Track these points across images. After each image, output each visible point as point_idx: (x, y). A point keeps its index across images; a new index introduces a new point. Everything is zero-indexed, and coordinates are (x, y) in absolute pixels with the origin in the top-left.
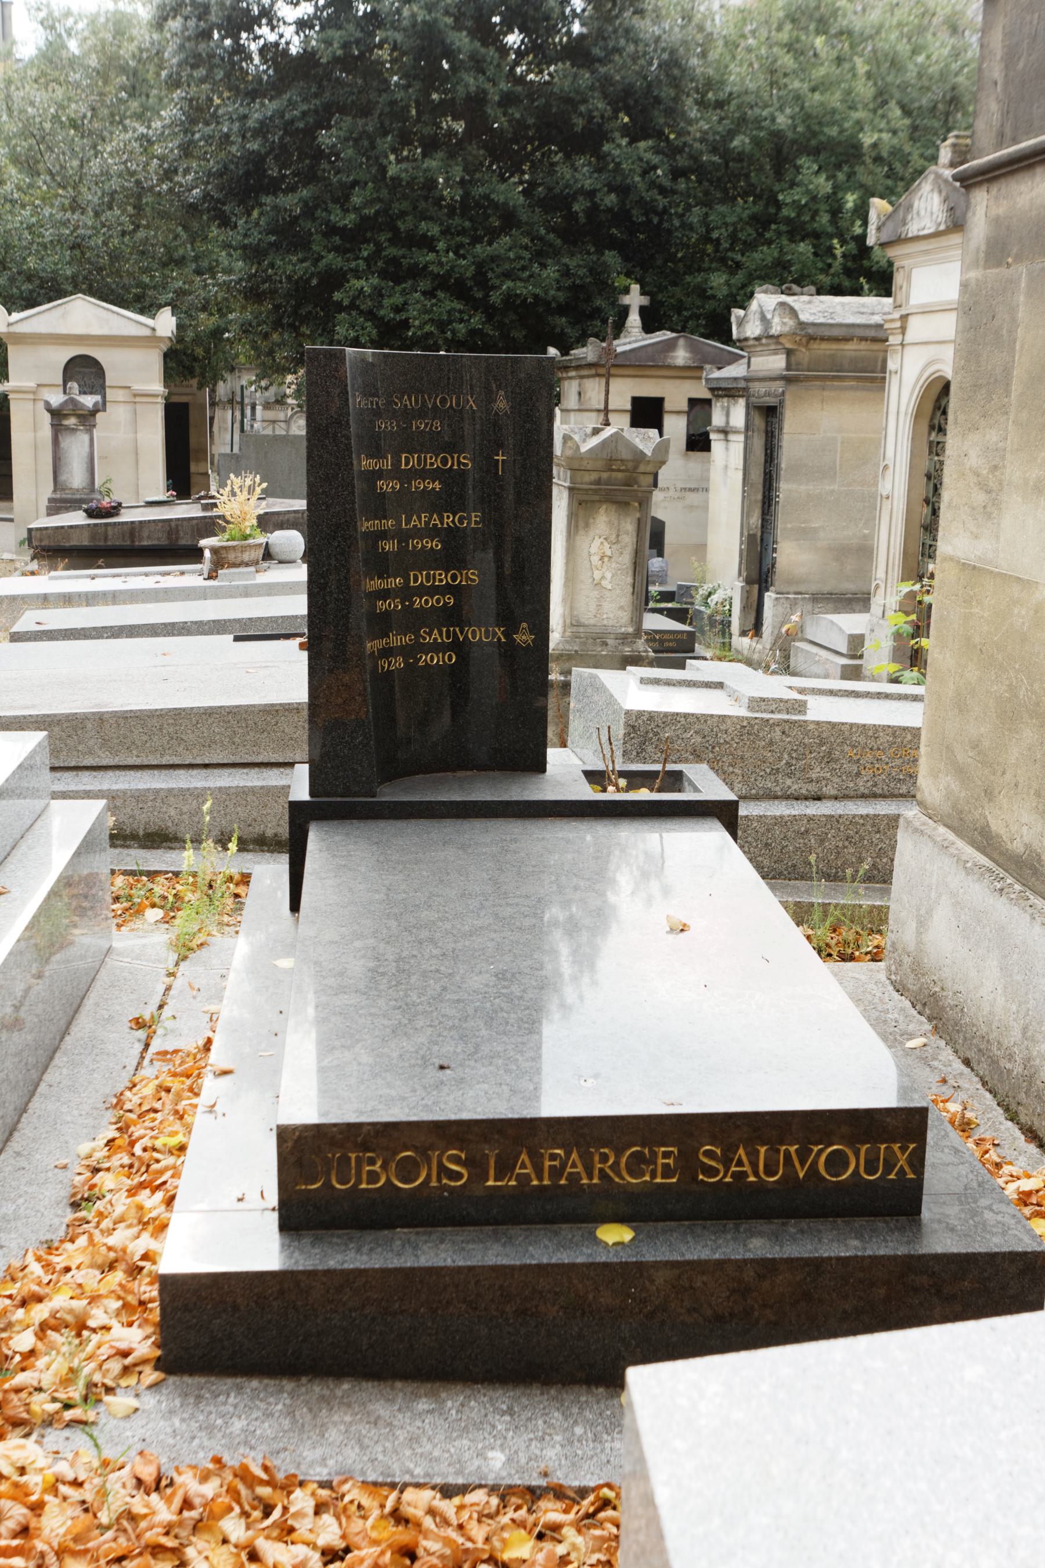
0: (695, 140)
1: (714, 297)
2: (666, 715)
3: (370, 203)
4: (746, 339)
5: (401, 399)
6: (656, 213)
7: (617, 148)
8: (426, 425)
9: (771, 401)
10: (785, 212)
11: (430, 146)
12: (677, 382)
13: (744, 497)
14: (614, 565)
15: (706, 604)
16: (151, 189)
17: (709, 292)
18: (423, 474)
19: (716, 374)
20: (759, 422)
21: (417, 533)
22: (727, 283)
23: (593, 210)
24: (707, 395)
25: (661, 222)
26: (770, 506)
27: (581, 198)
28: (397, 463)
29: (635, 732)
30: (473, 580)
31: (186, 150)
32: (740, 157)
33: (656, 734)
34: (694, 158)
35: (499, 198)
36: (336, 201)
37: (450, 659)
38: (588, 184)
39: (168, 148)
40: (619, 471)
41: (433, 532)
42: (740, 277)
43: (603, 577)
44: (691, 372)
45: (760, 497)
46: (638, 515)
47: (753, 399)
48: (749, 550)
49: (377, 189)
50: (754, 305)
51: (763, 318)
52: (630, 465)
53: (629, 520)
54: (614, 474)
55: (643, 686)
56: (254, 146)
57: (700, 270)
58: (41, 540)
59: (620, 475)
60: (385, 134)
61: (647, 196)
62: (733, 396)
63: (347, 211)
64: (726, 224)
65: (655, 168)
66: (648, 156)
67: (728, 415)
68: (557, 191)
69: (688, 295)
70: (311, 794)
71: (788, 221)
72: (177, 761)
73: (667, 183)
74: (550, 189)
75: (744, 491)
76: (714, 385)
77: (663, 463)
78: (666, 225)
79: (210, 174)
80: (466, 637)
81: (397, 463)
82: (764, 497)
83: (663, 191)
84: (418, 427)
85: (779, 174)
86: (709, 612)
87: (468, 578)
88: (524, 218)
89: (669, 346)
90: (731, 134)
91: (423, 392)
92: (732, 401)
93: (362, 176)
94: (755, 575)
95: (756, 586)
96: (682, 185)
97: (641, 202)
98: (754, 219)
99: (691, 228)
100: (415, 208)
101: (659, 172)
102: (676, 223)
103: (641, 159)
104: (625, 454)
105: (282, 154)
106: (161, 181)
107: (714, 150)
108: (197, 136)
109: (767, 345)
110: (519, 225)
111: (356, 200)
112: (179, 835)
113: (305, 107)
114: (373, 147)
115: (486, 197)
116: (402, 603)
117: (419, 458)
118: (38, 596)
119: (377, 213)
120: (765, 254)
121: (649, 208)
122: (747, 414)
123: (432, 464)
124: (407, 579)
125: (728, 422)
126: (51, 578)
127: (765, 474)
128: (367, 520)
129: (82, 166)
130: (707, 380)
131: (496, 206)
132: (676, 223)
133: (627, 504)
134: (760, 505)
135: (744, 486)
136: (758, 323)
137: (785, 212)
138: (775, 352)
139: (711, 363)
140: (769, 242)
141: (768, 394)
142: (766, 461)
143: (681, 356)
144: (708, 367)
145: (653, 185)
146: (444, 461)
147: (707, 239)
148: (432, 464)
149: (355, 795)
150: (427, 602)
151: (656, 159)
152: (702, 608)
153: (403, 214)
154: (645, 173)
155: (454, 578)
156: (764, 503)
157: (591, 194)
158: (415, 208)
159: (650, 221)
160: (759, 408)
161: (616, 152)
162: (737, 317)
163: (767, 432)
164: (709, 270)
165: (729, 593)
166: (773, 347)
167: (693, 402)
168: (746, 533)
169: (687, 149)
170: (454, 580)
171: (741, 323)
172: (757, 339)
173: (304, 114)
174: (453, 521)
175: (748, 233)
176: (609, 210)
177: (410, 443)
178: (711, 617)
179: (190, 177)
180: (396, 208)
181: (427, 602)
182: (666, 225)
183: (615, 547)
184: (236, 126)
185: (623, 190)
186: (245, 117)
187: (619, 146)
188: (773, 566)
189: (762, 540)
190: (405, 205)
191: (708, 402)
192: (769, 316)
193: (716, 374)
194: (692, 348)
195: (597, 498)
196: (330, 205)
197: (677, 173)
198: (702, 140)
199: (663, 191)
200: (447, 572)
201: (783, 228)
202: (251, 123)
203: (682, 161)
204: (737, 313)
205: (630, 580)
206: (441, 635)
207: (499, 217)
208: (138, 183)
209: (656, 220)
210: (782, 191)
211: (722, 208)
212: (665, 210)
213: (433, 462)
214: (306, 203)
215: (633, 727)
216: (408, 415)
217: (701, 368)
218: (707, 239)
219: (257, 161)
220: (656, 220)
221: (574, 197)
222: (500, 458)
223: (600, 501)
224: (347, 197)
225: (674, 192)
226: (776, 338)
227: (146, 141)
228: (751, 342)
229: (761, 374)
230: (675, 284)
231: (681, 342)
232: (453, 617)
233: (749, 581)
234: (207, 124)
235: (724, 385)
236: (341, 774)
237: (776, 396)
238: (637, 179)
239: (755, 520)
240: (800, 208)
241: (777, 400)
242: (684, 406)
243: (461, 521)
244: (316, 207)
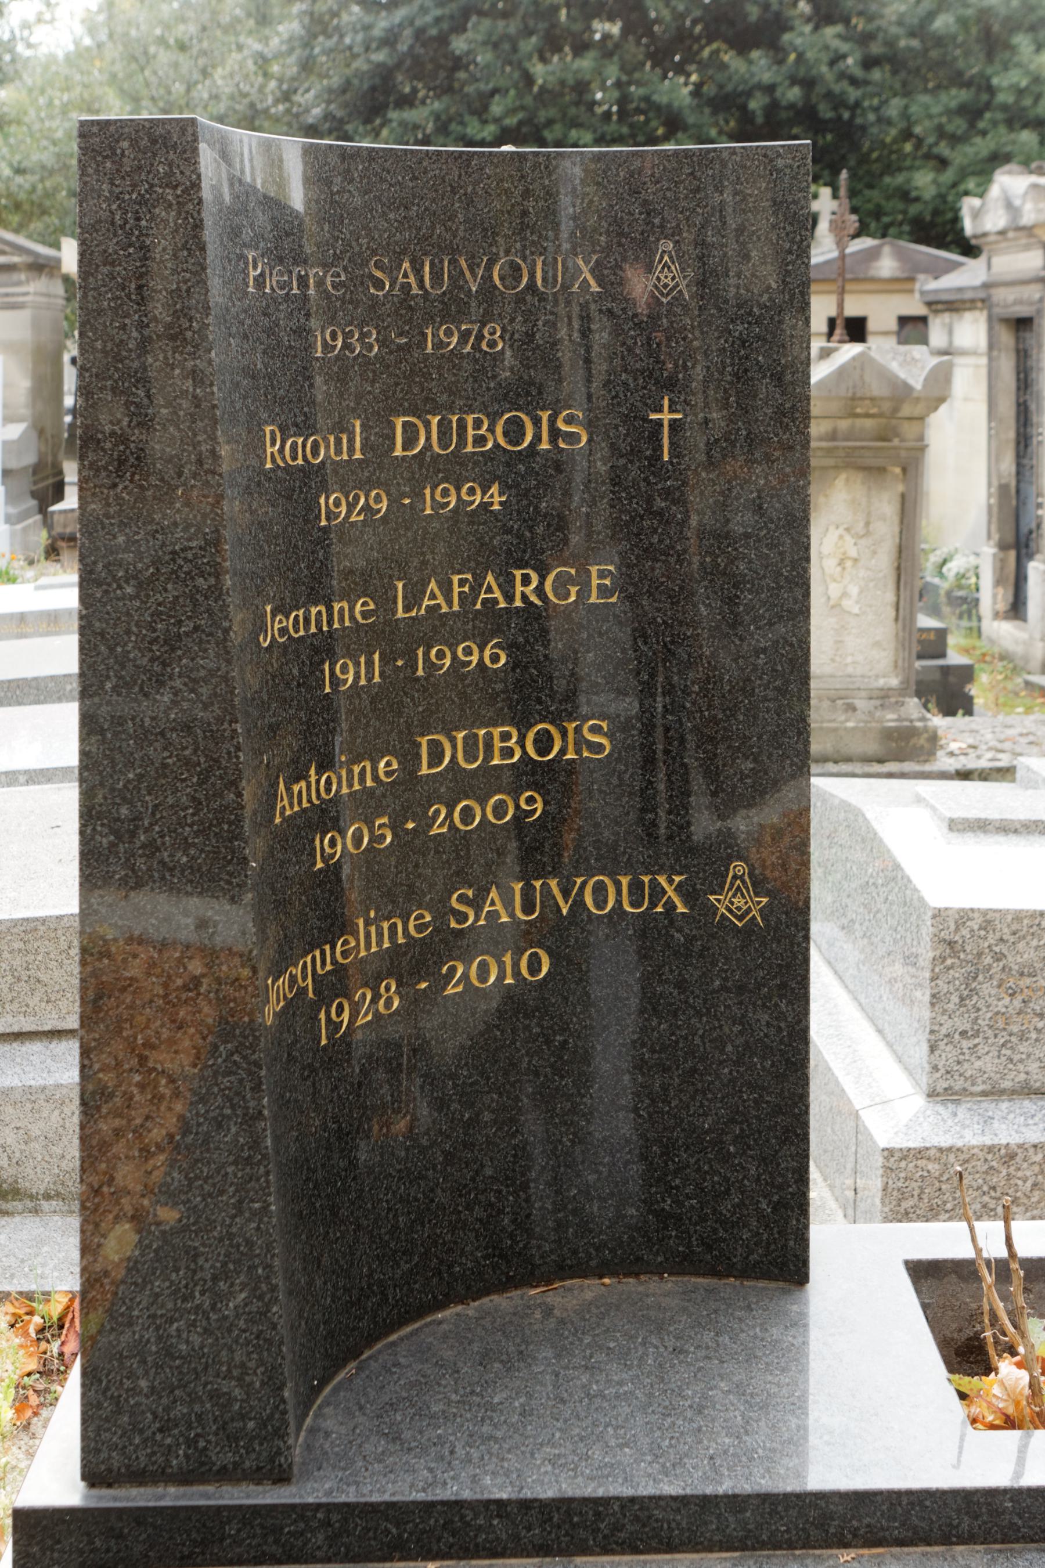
0: (890, 23)
1: (917, 199)
2: (1018, 916)
3: (513, 111)
4: (985, 235)
5: (391, 271)
6: (847, 107)
7: (801, 37)
8: (465, 336)
9: (1024, 311)
10: (1001, 98)
11: (581, 48)
12: (883, 297)
13: (990, 437)
14: (862, 573)
15: (941, 575)
16: (266, 111)
17: (914, 194)
18: (453, 468)
19: (933, 285)
20: (1006, 338)
21: (437, 628)
22: (935, 181)
23: (773, 108)
24: (920, 310)
25: (853, 117)
26: (1026, 446)
27: (758, 94)
28: (378, 446)
29: (955, 954)
30: (599, 748)
31: (307, 66)
32: (939, 41)
33: (999, 957)
34: (890, 43)
35: (661, 99)
36: (473, 113)
37: (534, 966)
38: (767, 77)
39: (287, 67)
40: (867, 416)
41: (488, 623)
42: (948, 176)
43: (845, 594)
44: (903, 283)
45: (1012, 434)
46: (900, 488)
47: (997, 310)
48: (1001, 506)
49: (520, 95)
50: (995, 191)
51: (1009, 205)
52: (886, 406)
53: (886, 496)
54: (859, 422)
55: (955, 838)
56: (380, 56)
57: (900, 169)
58: (65, 526)
59: (869, 423)
60: (530, 33)
61: (837, 88)
62: (956, 310)
63: (485, 122)
64: (930, 117)
65: (844, 57)
66: (836, 43)
67: (950, 333)
68: (729, 88)
69: (888, 198)
70: (93, 1475)
71: (1004, 108)
72: (28, 1026)
73: (858, 72)
74: (721, 87)
75: (990, 429)
76: (931, 298)
77: (942, 400)
78: (859, 121)
79: (330, 91)
80: (579, 904)
81: (378, 446)
82: (1018, 434)
83: (854, 82)
84: (439, 345)
85: (990, 56)
86: (945, 586)
87: (581, 742)
88: (691, 120)
89: (873, 255)
90: (931, 15)
91: (454, 252)
92: (955, 316)
93: (502, 83)
94: (1010, 538)
95: (1012, 554)
96: (876, 75)
97: (829, 95)
98: (962, 110)
99: (889, 122)
100: (564, 115)
101: (850, 61)
102: (871, 117)
103: (827, 48)
104: (877, 388)
105: (416, 68)
106: (277, 102)
107: (912, 34)
108: (317, 50)
109: (1015, 239)
110: (685, 128)
111: (496, 108)
112: (22, 1184)
113: (439, 12)
114: (515, 49)
115: (647, 99)
116: (396, 827)
117: (444, 428)
118: (11, 616)
119: (521, 123)
120: (981, 146)
121: (838, 102)
122: (991, 329)
123: (480, 440)
124: (409, 758)
125: (951, 342)
126: (38, 588)
127: (1019, 405)
128: (282, 609)
129: (188, 91)
130: (922, 293)
131: (658, 108)
132: (871, 117)
133: (882, 470)
134: (1012, 445)
135: (990, 421)
136: (1001, 212)
137: (1001, 98)
138: (1027, 248)
139: (926, 271)
140: (984, 133)
141: (1018, 302)
142: (1018, 389)
143: (887, 265)
144: (921, 277)
145: (842, 75)
146: (514, 431)
147: (907, 134)
148: (480, 440)
149: (225, 1475)
150: (467, 815)
151: (844, 47)
152: (936, 581)
153: (550, 123)
154: (832, 63)
155: (544, 743)
156: (1018, 443)
157: (770, 89)
158: (564, 115)
159: (840, 118)
160: (1006, 321)
161: (799, 41)
162: (972, 209)
163: (1018, 351)
164: (910, 168)
165: (973, 560)
166: (1024, 241)
167: (904, 321)
168: (995, 483)
169: (881, 35)
170: (543, 751)
171: (976, 215)
172: (1002, 233)
173: (438, 20)
174: (540, 591)
175: (958, 125)
176: (792, 106)
177: (410, 383)
178: (949, 594)
179: (308, 96)
180: (543, 115)
181: (467, 815)
182: (859, 121)
183: (863, 542)
184: (360, 37)
185: (808, 83)
186: (367, 28)
187: (802, 34)
188: (1039, 526)
189: (1018, 491)
190: (552, 112)
191: (923, 320)
192: (1017, 202)
193: (933, 285)
194: (900, 256)
195: (831, 462)
196: (467, 118)
197: (869, 63)
198: (900, 23)
199: (854, 82)
200: (523, 725)
201: (1000, 116)
202: (377, 33)
203: (876, 49)
204: (969, 205)
205: (890, 597)
206: (508, 904)
207: (664, 124)
208: (252, 105)
209: (846, 115)
210: (997, 73)
211: (925, 99)
212: (857, 104)
213: (484, 433)
214: (437, 117)
215: (951, 944)
216: (409, 311)
217: (911, 279)
218: (907, 134)
219: (385, 76)
220: (846, 115)
221: (749, 94)
222: (666, 417)
223: (836, 467)
224: (486, 108)
225: (866, 83)
226: (1028, 230)
227: (263, 61)
228: (992, 238)
229: (1008, 278)
230: (870, 186)
231: (887, 250)
232: (536, 849)
233: (1003, 546)
234: (329, 37)
235: (944, 297)
236: (180, 1410)
237: (1031, 304)
238: (824, 69)
239: (1008, 465)
240: (1020, 92)
241: (1034, 308)
242: (893, 325)
243: (562, 585)
244: (450, 120)
